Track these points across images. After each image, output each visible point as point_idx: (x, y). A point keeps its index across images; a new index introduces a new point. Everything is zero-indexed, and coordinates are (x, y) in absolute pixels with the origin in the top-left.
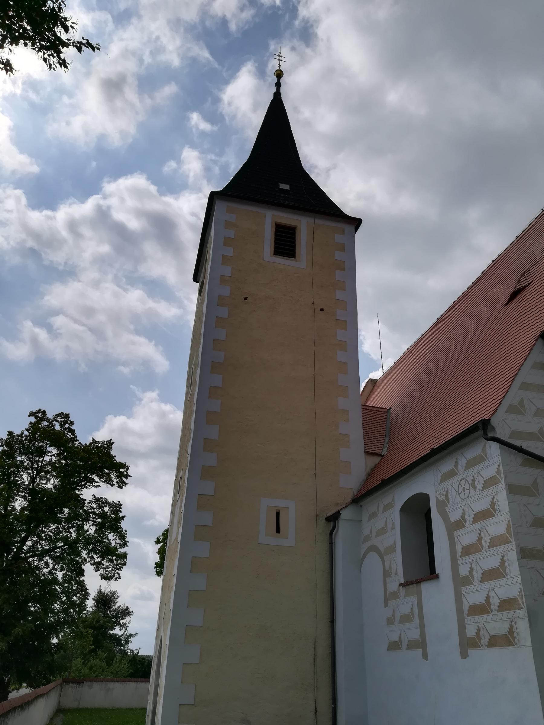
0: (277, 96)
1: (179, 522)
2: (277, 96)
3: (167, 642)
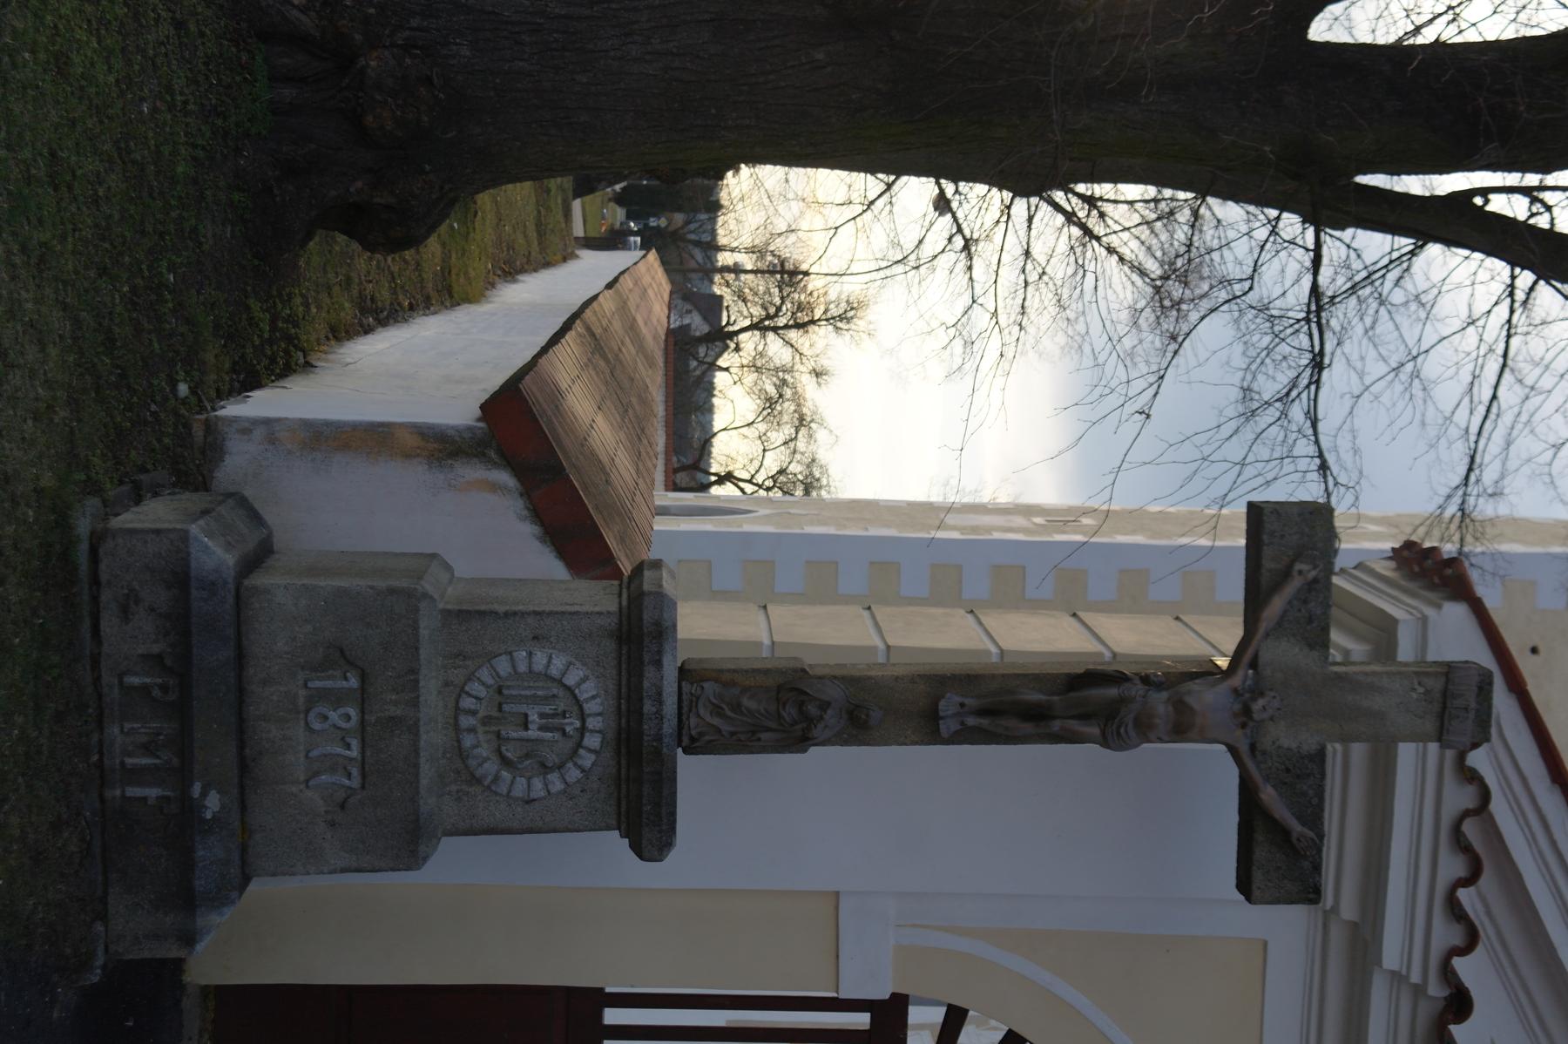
1: (975, 529)
3: (747, 528)
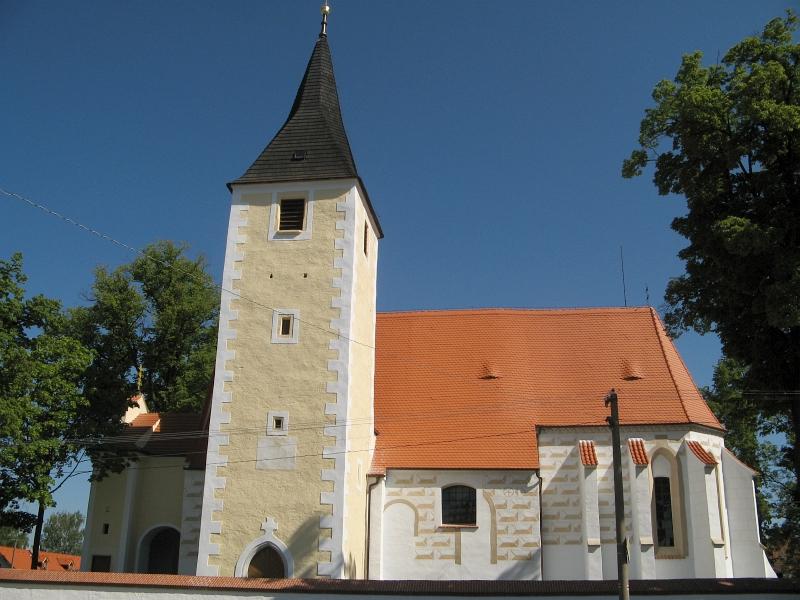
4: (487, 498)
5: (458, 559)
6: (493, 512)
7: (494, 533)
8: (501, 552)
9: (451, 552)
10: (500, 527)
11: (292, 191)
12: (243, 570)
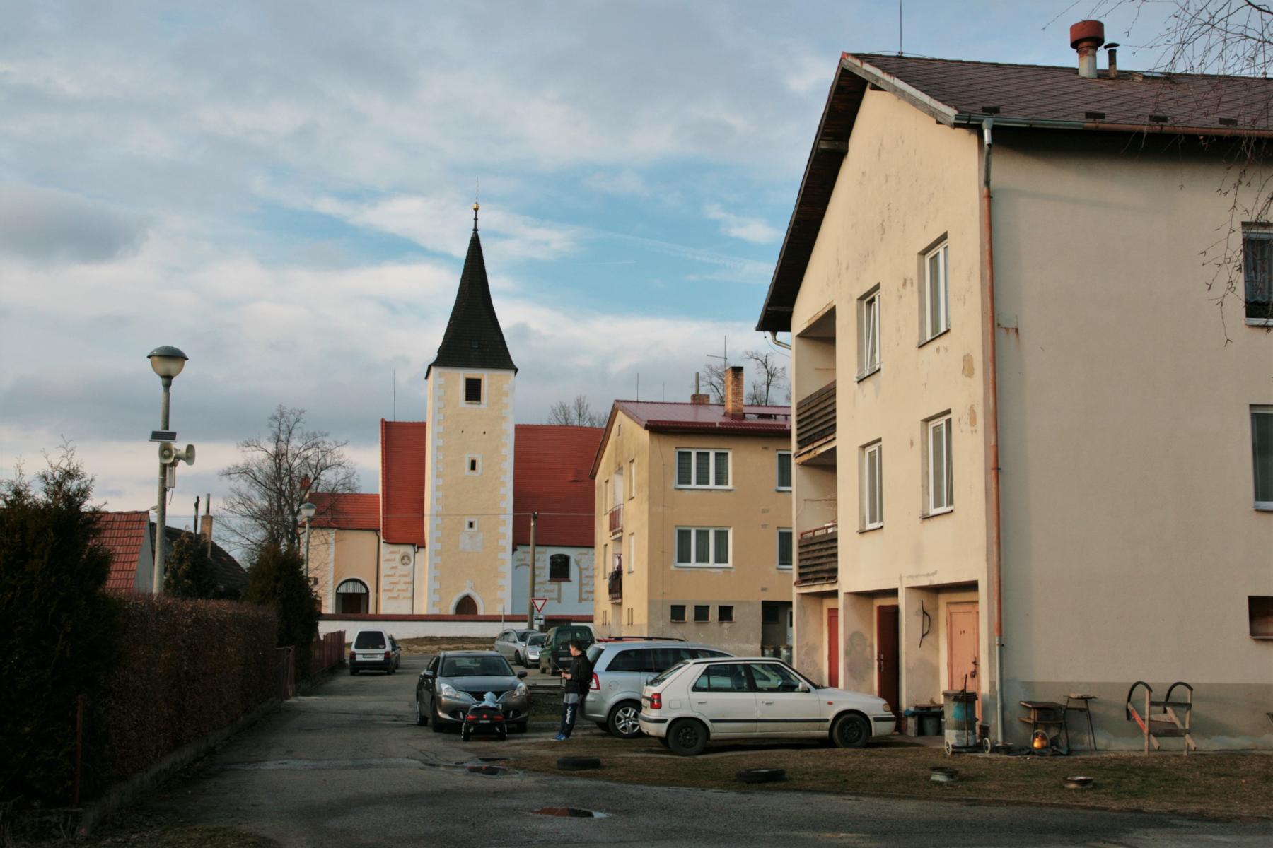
0: (475, 230)
2: (475, 230)
4: (577, 562)
5: (559, 600)
6: (581, 570)
7: (581, 585)
8: (585, 596)
9: (555, 595)
10: (584, 581)
11: (474, 373)
12: (451, 611)
